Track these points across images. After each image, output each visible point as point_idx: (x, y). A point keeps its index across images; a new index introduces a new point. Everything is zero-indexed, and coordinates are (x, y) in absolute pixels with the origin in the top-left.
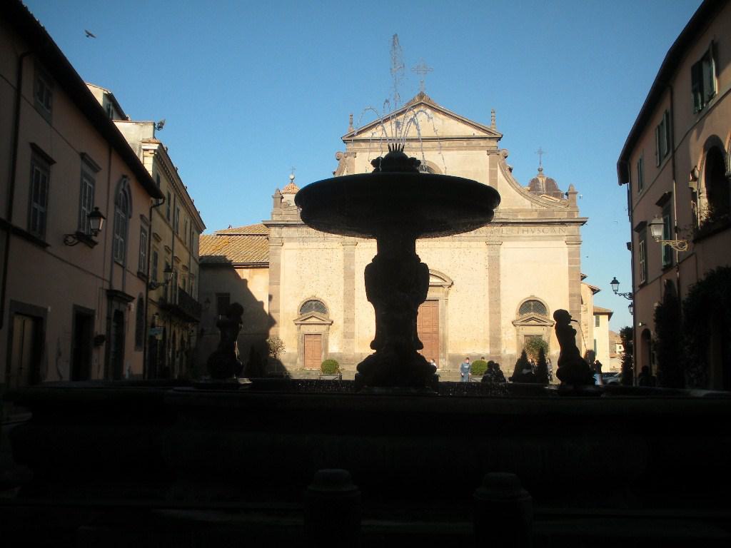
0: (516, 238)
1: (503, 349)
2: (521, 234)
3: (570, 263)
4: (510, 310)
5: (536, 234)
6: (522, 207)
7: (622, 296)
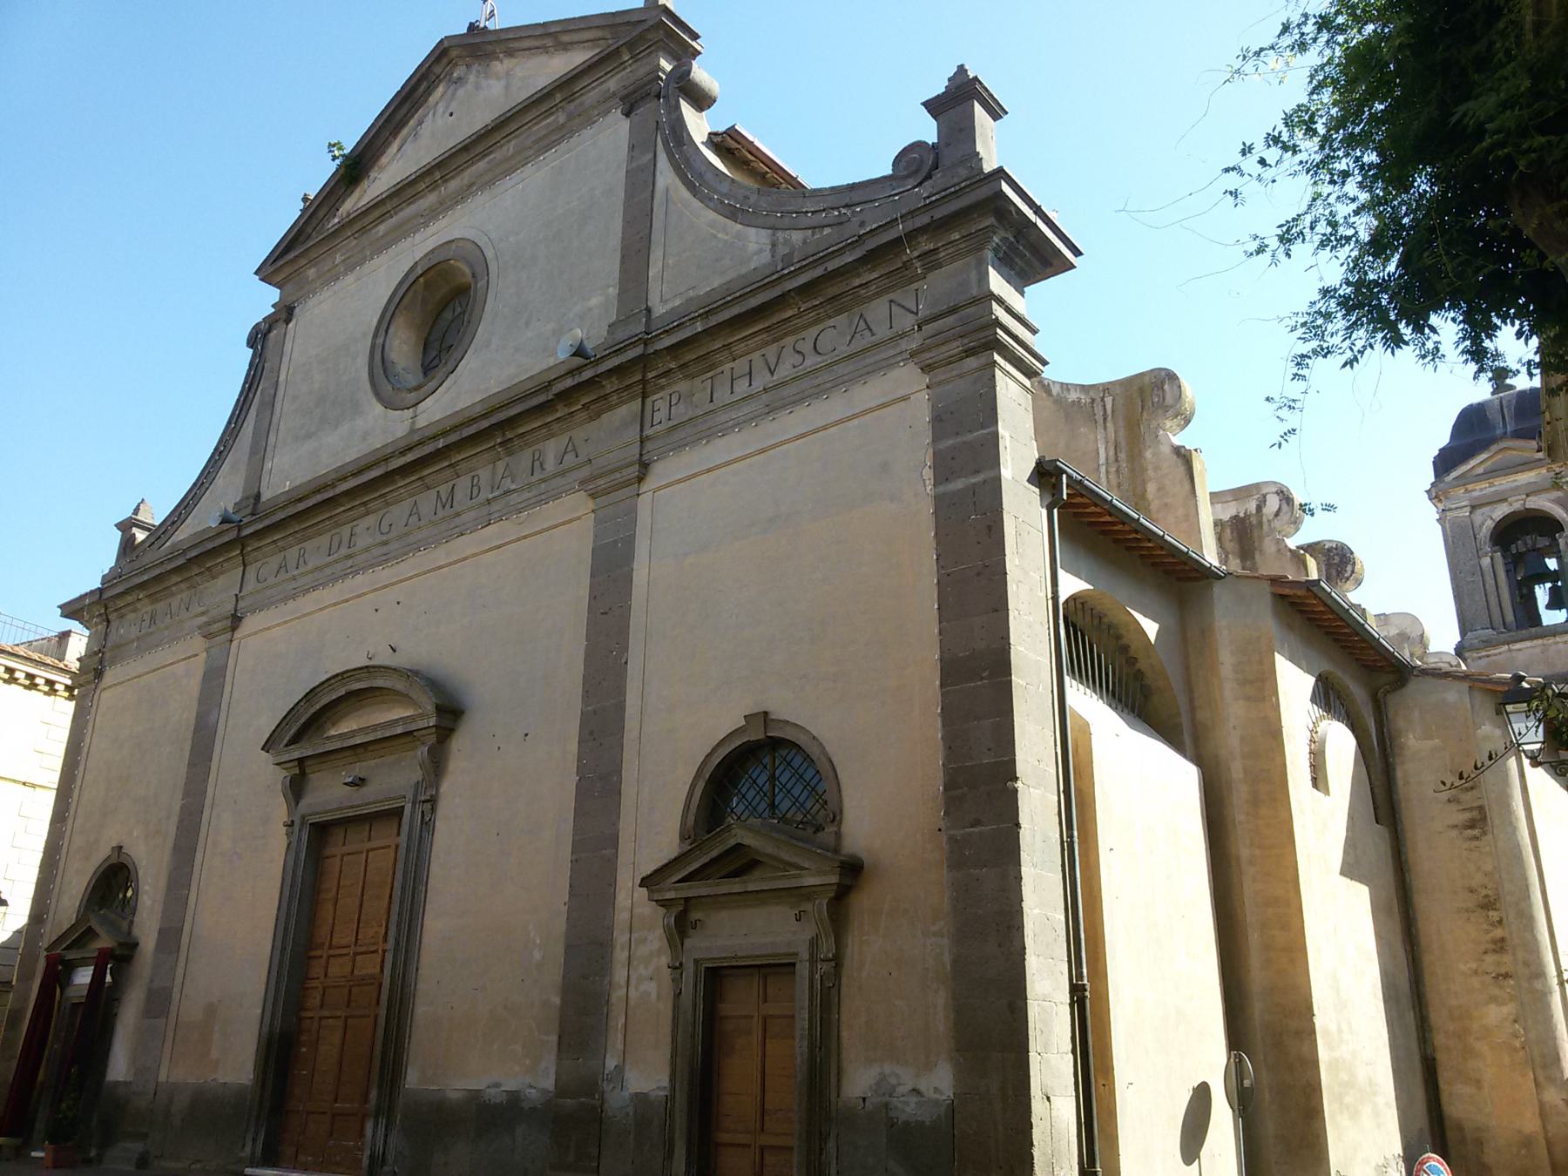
0: (698, 430)
1: (611, 1063)
4: (654, 826)
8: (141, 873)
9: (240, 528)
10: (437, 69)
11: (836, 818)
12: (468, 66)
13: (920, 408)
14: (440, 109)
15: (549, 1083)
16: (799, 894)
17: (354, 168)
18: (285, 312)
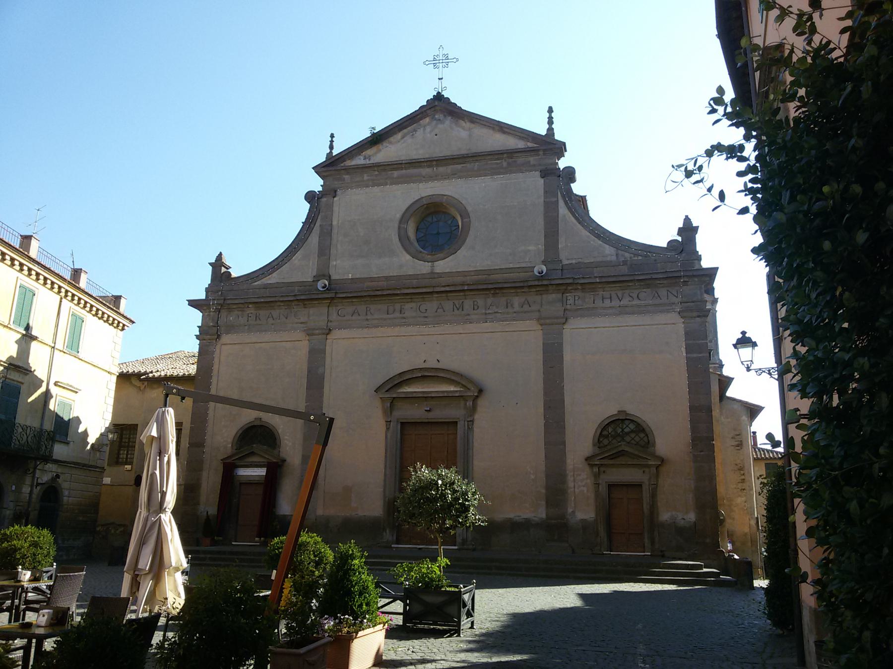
0: (591, 312)
1: (570, 510)
2: (599, 303)
3: (688, 350)
4: (580, 443)
5: (625, 302)
6: (599, 259)
7: (765, 376)
8: (280, 431)
9: (336, 293)
10: (429, 112)
11: (654, 445)
12: (445, 116)
13: (680, 328)
14: (428, 129)
15: (544, 516)
16: (648, 466)
17: (377, 139)
18: (329, 191)
